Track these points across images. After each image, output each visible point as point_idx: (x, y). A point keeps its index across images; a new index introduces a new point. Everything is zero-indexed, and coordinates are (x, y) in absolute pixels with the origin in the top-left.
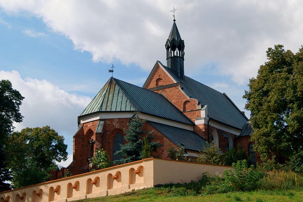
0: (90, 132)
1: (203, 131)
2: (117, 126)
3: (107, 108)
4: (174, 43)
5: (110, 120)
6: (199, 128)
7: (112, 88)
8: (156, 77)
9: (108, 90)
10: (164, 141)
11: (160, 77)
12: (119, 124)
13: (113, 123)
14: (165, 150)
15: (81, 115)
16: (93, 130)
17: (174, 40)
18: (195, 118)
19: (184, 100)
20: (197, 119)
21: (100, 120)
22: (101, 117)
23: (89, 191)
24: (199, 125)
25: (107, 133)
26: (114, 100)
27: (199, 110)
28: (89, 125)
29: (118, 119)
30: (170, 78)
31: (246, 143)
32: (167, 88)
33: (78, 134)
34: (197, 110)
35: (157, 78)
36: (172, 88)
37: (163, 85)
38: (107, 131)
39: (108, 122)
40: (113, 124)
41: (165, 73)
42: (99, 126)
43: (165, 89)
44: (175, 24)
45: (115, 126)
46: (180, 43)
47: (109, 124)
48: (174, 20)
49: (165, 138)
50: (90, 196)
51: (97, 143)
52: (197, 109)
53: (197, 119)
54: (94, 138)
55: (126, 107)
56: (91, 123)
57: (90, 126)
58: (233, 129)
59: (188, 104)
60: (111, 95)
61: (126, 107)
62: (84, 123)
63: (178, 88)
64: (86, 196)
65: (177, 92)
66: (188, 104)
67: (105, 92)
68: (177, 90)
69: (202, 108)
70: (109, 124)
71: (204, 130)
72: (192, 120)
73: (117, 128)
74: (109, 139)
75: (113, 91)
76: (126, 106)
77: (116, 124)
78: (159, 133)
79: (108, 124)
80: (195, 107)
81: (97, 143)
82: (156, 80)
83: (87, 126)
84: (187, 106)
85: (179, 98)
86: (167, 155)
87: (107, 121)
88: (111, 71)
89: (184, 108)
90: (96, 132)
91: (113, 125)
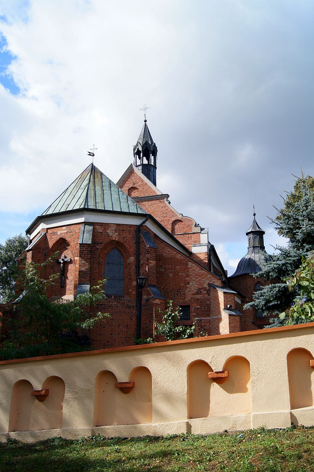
0: (62, 244)
1: (206, 263)
2: (115, 236)
3: (97, 205)
4: (147, 147)
5: (101, 224)
6: (199, 257)
7: (98, 178)
8: (128, 185)
9: (92, 180)
10: (189, 268)
11: (135, 186)
12: (117, 234)
13: (108, 231)
14: (191, 282)
15: (44, 214)
16: (68, 239)
17: (147, 143)
18: (191, 244)
19: (173, 219)
20: (195, 245)
21: (85, 223)
22: (87, 219)
23: (198, 406)
24: (199, 253)
25: (98, 247)
26: (106, 195)
27: (198, 233)
28: (61, 233)
29: (116, 225)
30: (150, 188)
31: (251, 283)
32: (145, 201)
33: (38, 245)
34: (194, 233)
35: (130, 187)
36: (154, 202)
37: (140, 197)
38: (98, 243)
39: (100, 229)
40: (107, 233)
41: (142, 181)
42: (84, 233)
43: (142, 201)
44: (146, 125)
45: (111, 236)
46: (154, 149)
47: (100, 232)
48: (145, 121)
49: (191, 263)
50: (200, 427)
51: (82, 262)
52: (193, 231)
53: (195, 245)
54: (68, 254)
55: (129, 208)
56: (64, 228)
57: (61, 234)
58: (217, 263)
59: (178, 225)
60: (98, 188)
61: (129, 208)
62: (48, 229)
63: (163, 202)
64: (189, 426)
65: (162, 207)
66: (178, 225)
67: (86, 182)
68: (162, 205)
69: (201, 231)
70: (101, 231)
71: (207, 261)
72: (186, 246)
73: (114, 239)
74: (100, 256)
75: (100, 182)
76: (129, 206)
77: (113, 234)
78: (179, 255)
79: (99, 231)
80: (191, 229)
81: (82, 262)
82: (128, 188)
83: (54, 233)
84: (176, 227)
85: (165, 215)
86: (196, 291)
87: (97, 227)
88: (91, 154)
89: (173, 229)
90: (81, 243)
91: (108, 235)
